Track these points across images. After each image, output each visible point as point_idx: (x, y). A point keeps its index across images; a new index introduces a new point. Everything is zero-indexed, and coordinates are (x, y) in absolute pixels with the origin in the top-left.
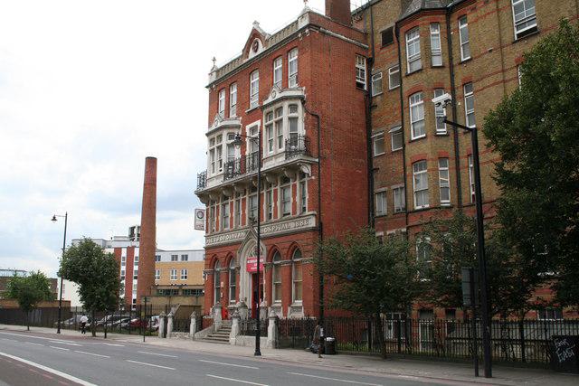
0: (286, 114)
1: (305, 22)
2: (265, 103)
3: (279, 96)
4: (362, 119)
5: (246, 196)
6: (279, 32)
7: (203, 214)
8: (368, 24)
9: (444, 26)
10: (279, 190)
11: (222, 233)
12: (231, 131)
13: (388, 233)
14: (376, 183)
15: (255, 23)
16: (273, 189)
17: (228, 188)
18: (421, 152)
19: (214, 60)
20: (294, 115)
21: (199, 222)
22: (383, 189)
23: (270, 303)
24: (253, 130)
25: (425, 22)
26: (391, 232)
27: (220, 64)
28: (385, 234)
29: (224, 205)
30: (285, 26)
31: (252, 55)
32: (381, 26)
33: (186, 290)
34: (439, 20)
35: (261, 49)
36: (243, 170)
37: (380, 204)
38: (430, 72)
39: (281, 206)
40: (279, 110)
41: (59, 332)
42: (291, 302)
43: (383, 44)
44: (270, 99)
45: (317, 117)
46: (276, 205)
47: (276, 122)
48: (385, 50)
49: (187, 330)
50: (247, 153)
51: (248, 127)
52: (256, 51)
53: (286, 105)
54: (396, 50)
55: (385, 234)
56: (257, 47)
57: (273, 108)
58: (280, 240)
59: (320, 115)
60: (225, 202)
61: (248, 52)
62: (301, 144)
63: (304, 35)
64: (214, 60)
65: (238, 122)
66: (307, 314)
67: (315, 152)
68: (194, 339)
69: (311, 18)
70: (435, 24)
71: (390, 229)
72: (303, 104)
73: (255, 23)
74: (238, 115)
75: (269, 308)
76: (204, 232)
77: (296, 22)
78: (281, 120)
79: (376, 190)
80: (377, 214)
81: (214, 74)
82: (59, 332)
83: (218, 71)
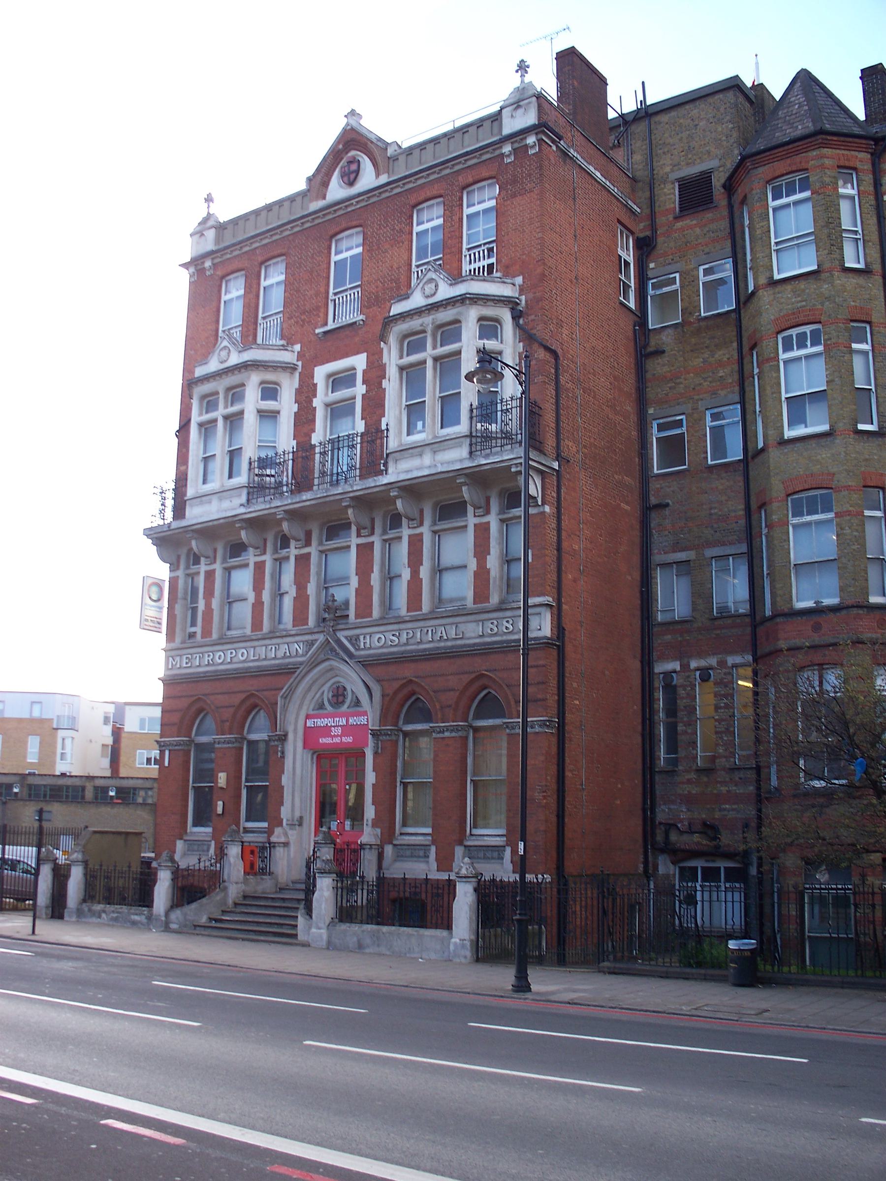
0: (252, 400)
1: (529, 118)
2: (199, 372)
3: (235, 359)
4: (630, 381)
5: (313, 550)
6: (435, 141)
7: (161, 589)
8: (637, 157)
9: (868, 178)
10: (314, 559)
11: (223, 641)
12: (270, 376)
13: (693, 664)
14: (658, 540)
15: (353, 113)
16: (203, 568)
17: (257, 524)
18: (816, 469)
19: (209, 199)
20: (270, 405)
21: (151, 612)
22: (681, 556)
23: (388, 836)
24: (338, 381)
25: (827, 162)
26: (703, 663)
27: (225, 213)
28: (685, 667)
29: (280, 561)
30: (449, 127)
31: (336, 191)
32: (676, 166)
33: (37, 787)
34: (859, 165)
35: (368, 179)
36: (302, 482)
37: (669, 594)
38: (840, 280)
39: (273, 600)
40: (236, 394)
41: (522, 985)
42: (182, 832)
43: (682, 209)
44: (213, 365)
45: (554, 353)
46: (208, 605)
47: (226, 418)
48: (687, 222)
49: (145, 899)
50: (316, 439)
51: (320, 373)
52: (351, 184)
53: (471, 316)
54: (725, 224)
55: (685, 667)
56: (357, 172)
57: (220, 386)
58: (426, 667)
59: (559, 351)
60: (392, 534)
61: (325, 184)
62: (514, 421)
63: (521, 152)
64: (209, 199)
65: (289, 357)
66: (522, 865)
67: (550, 442)
68: (166, 928)
69: (540, 109)
70: (847, 170)
71: (700, 655)
72: (517, 316)
73: (353, 113)
74: (288, 339)
75: (389, 850)
76: (162, 637)
77: (496, 117)
78: (241, 413)
79: (658, 558)
80: (660, 617)
81: (211, 234)
82: (522, 985)
83: (221, 228)
